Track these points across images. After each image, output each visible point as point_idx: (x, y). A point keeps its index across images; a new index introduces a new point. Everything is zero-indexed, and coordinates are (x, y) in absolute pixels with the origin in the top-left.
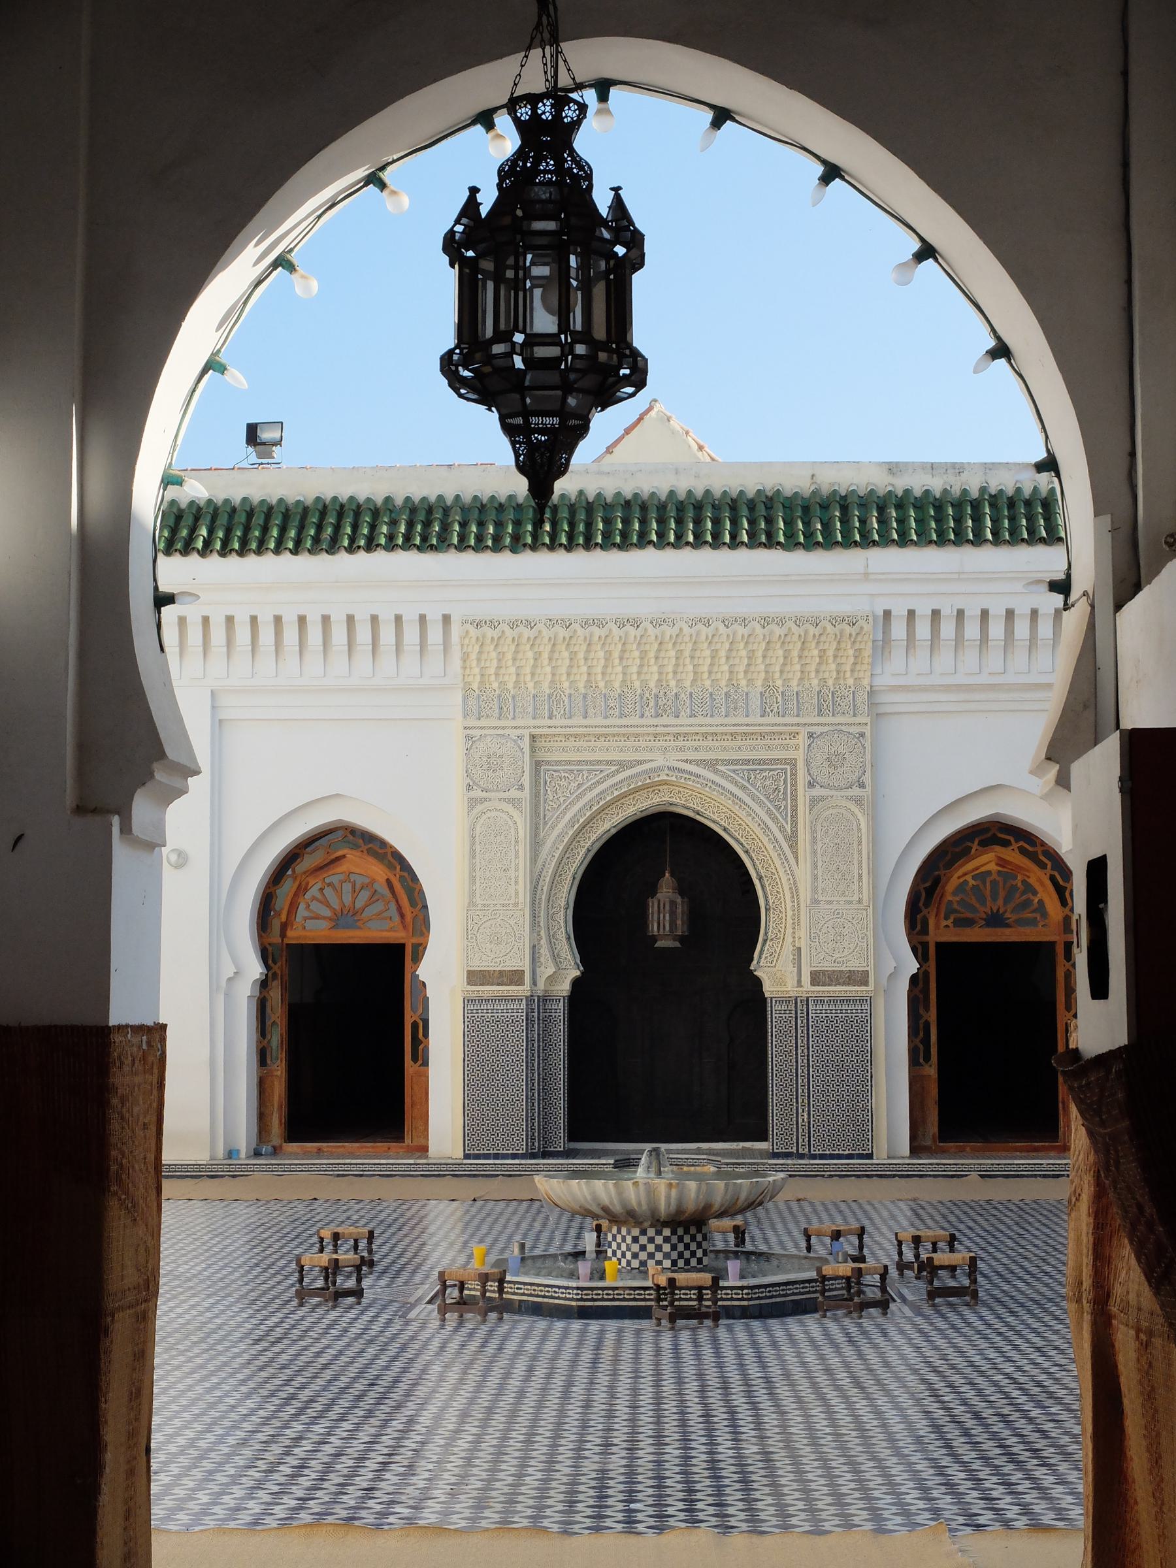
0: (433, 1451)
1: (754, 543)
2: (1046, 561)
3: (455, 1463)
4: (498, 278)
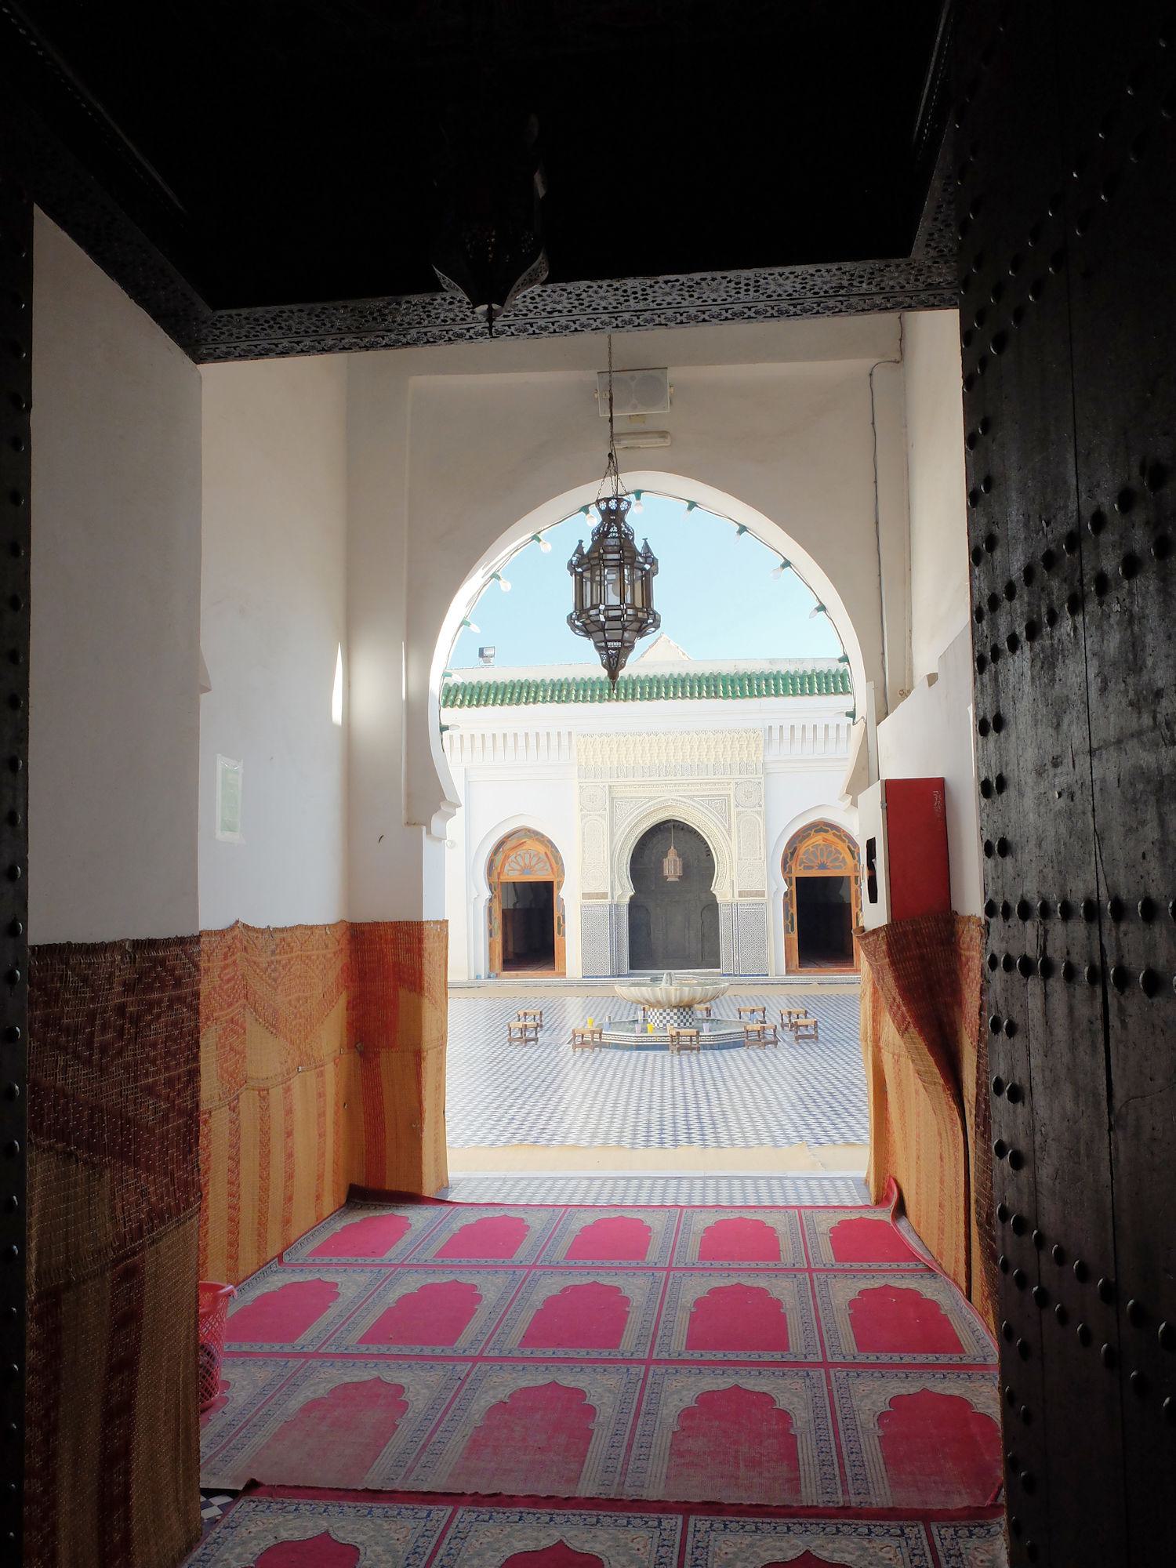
0: (571, 1112)
1: (709, 696)
2: (844, 702)
3: (581, 1117)
4: (592, 580)
